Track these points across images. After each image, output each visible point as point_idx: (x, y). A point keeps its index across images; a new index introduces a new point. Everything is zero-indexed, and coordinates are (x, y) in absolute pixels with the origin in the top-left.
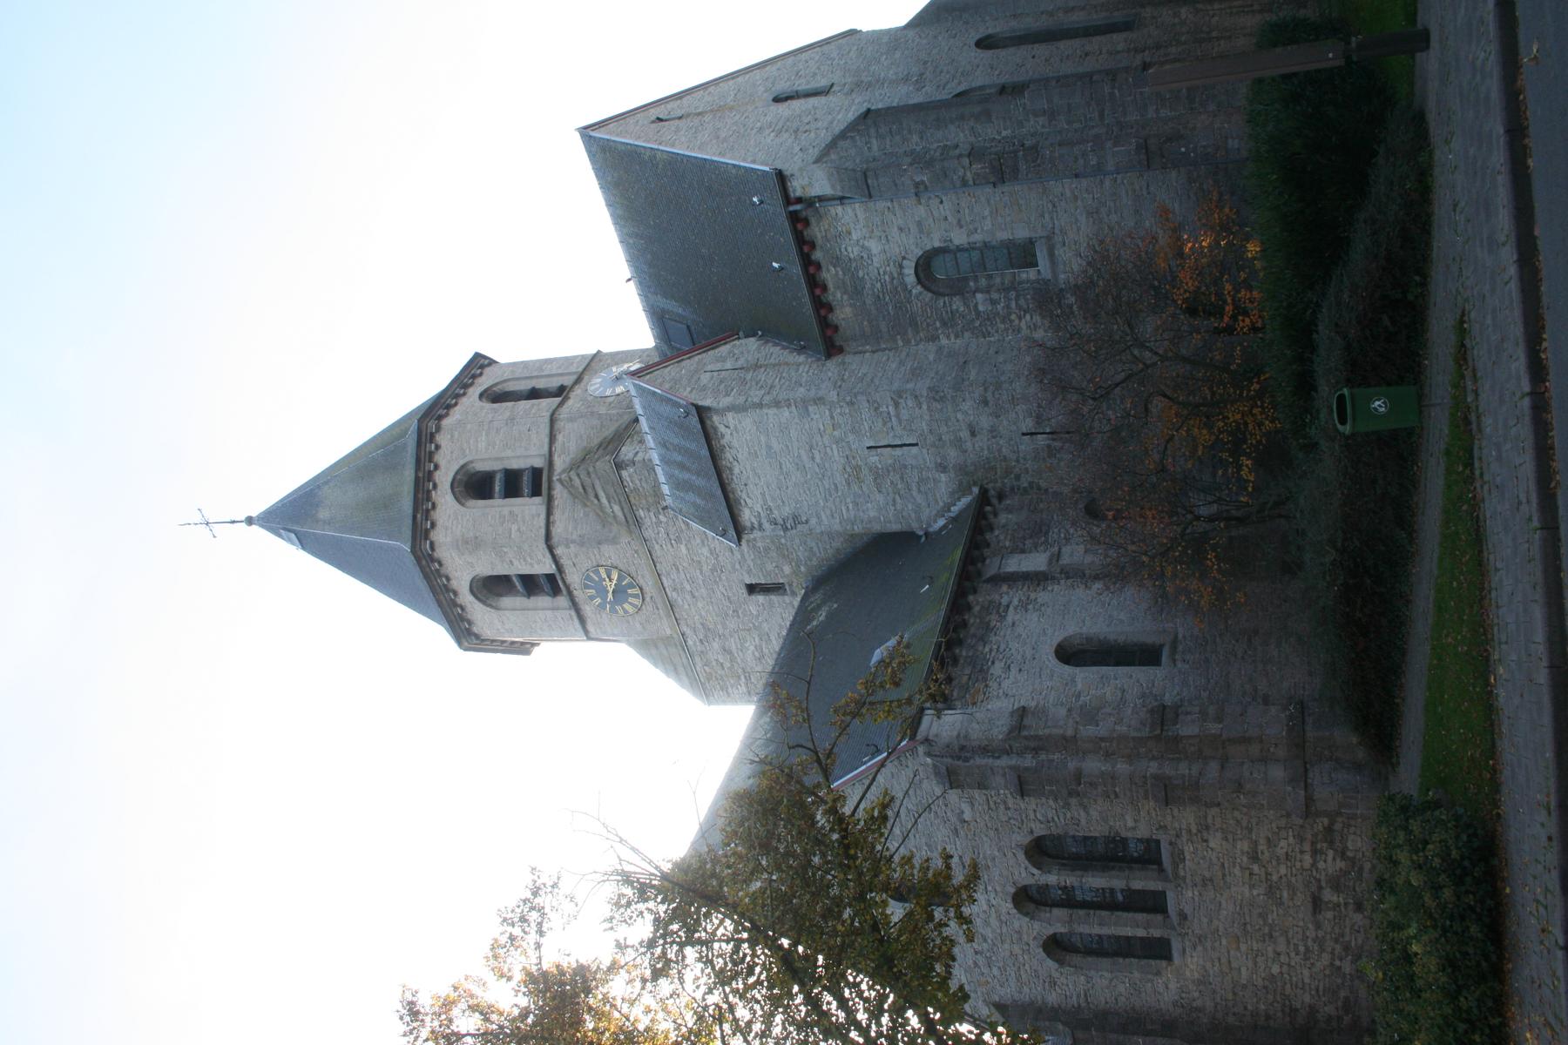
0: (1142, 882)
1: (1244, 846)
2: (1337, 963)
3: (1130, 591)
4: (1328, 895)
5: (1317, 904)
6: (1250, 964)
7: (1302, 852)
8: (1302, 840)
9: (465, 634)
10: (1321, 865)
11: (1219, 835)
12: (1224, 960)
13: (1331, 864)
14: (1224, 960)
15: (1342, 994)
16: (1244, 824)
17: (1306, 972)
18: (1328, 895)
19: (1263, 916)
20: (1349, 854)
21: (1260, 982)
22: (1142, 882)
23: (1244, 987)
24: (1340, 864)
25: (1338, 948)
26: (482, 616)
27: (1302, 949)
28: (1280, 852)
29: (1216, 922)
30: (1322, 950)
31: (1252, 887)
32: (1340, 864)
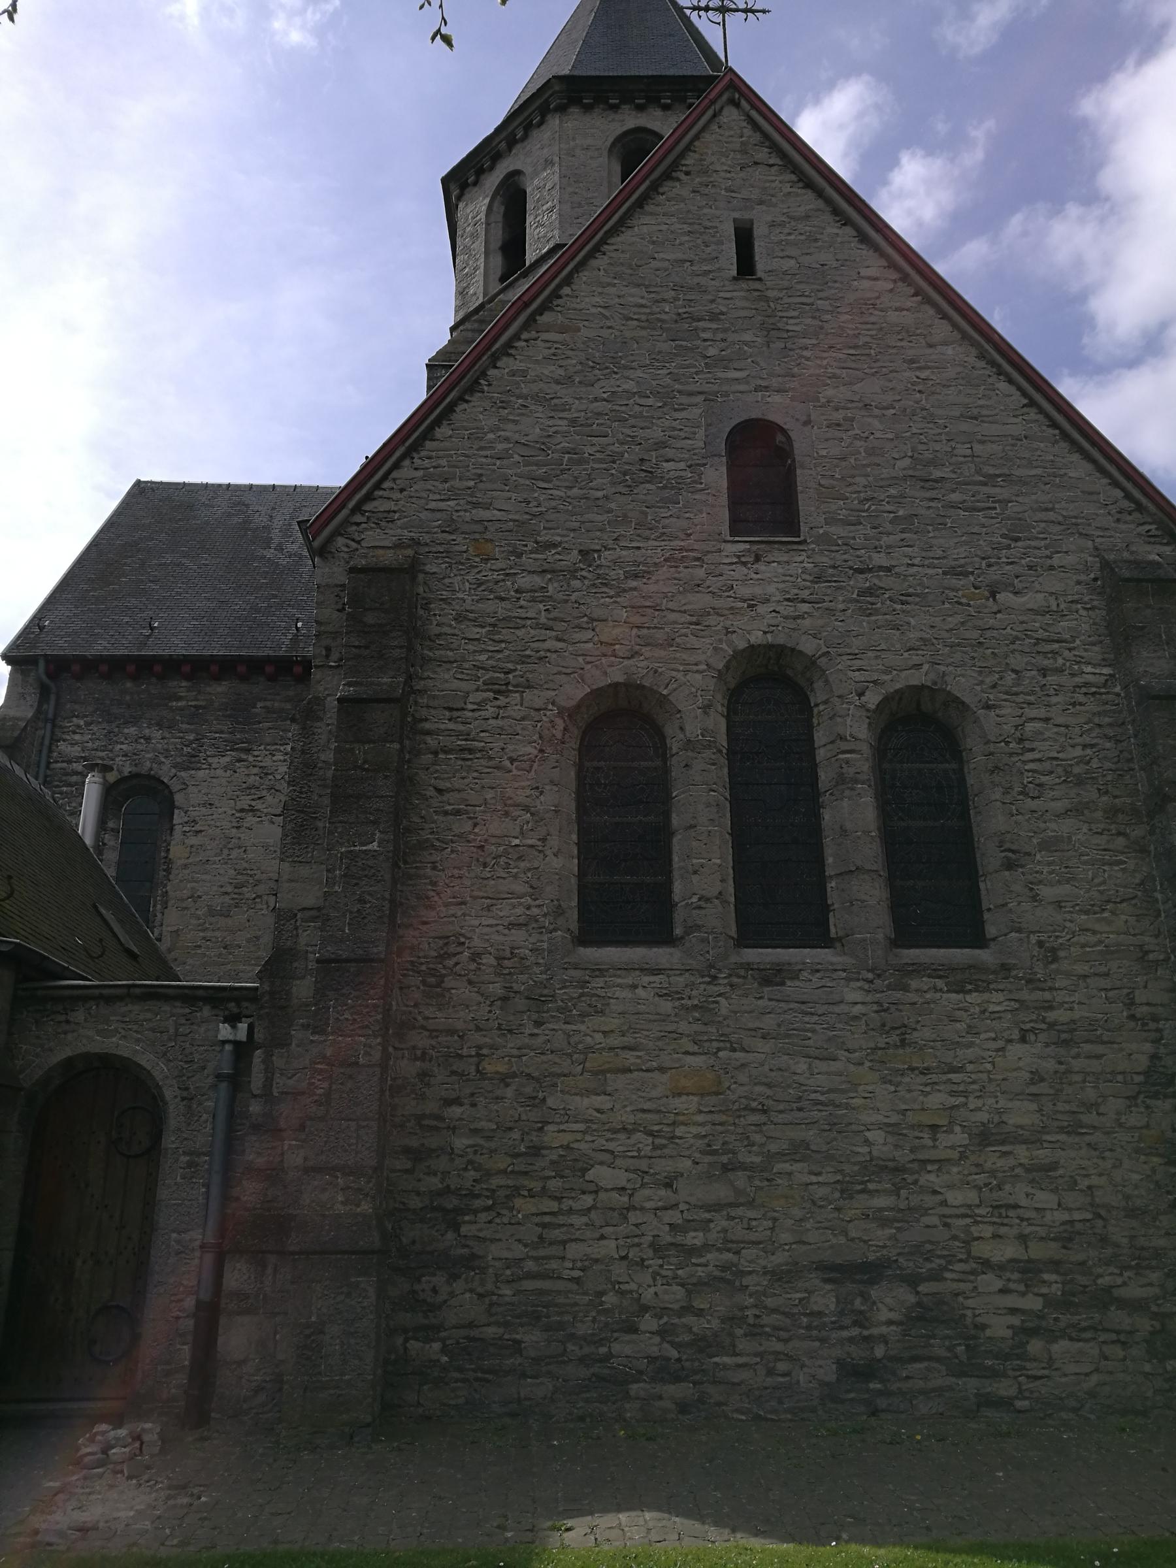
0: (703, 866)
1: (1022, 1115)
2: (649, 1323)
3: (9, 667)
4: (889, 1303)
5: (857, 1273)
6: (626, 1117)
7: (1023, 1239)
8: (1066, 1240)
9: (457, 184)
10: (990, 1282)
11: (1050, 1065)
12: (630, 1058)
13: (995, 1308)
14: (630, 1058)
15: (532, 1338)
16: (1090, 1118)
17: (609, 1248)
18: (889, 1303)
19: (798, 1151)
20: (1035, 1346)
21: (553, 1136)
22: (703, 866)
23: (535, 1102)
24: (1000, 1328)
25: (709, 1325)
26: (477, 206)
27: (695, 1238)
28: (1019, 1192)
29: (767, 1047)
30: (693, 1288)
31: (892, 1129)
32: (1000, 1328)
